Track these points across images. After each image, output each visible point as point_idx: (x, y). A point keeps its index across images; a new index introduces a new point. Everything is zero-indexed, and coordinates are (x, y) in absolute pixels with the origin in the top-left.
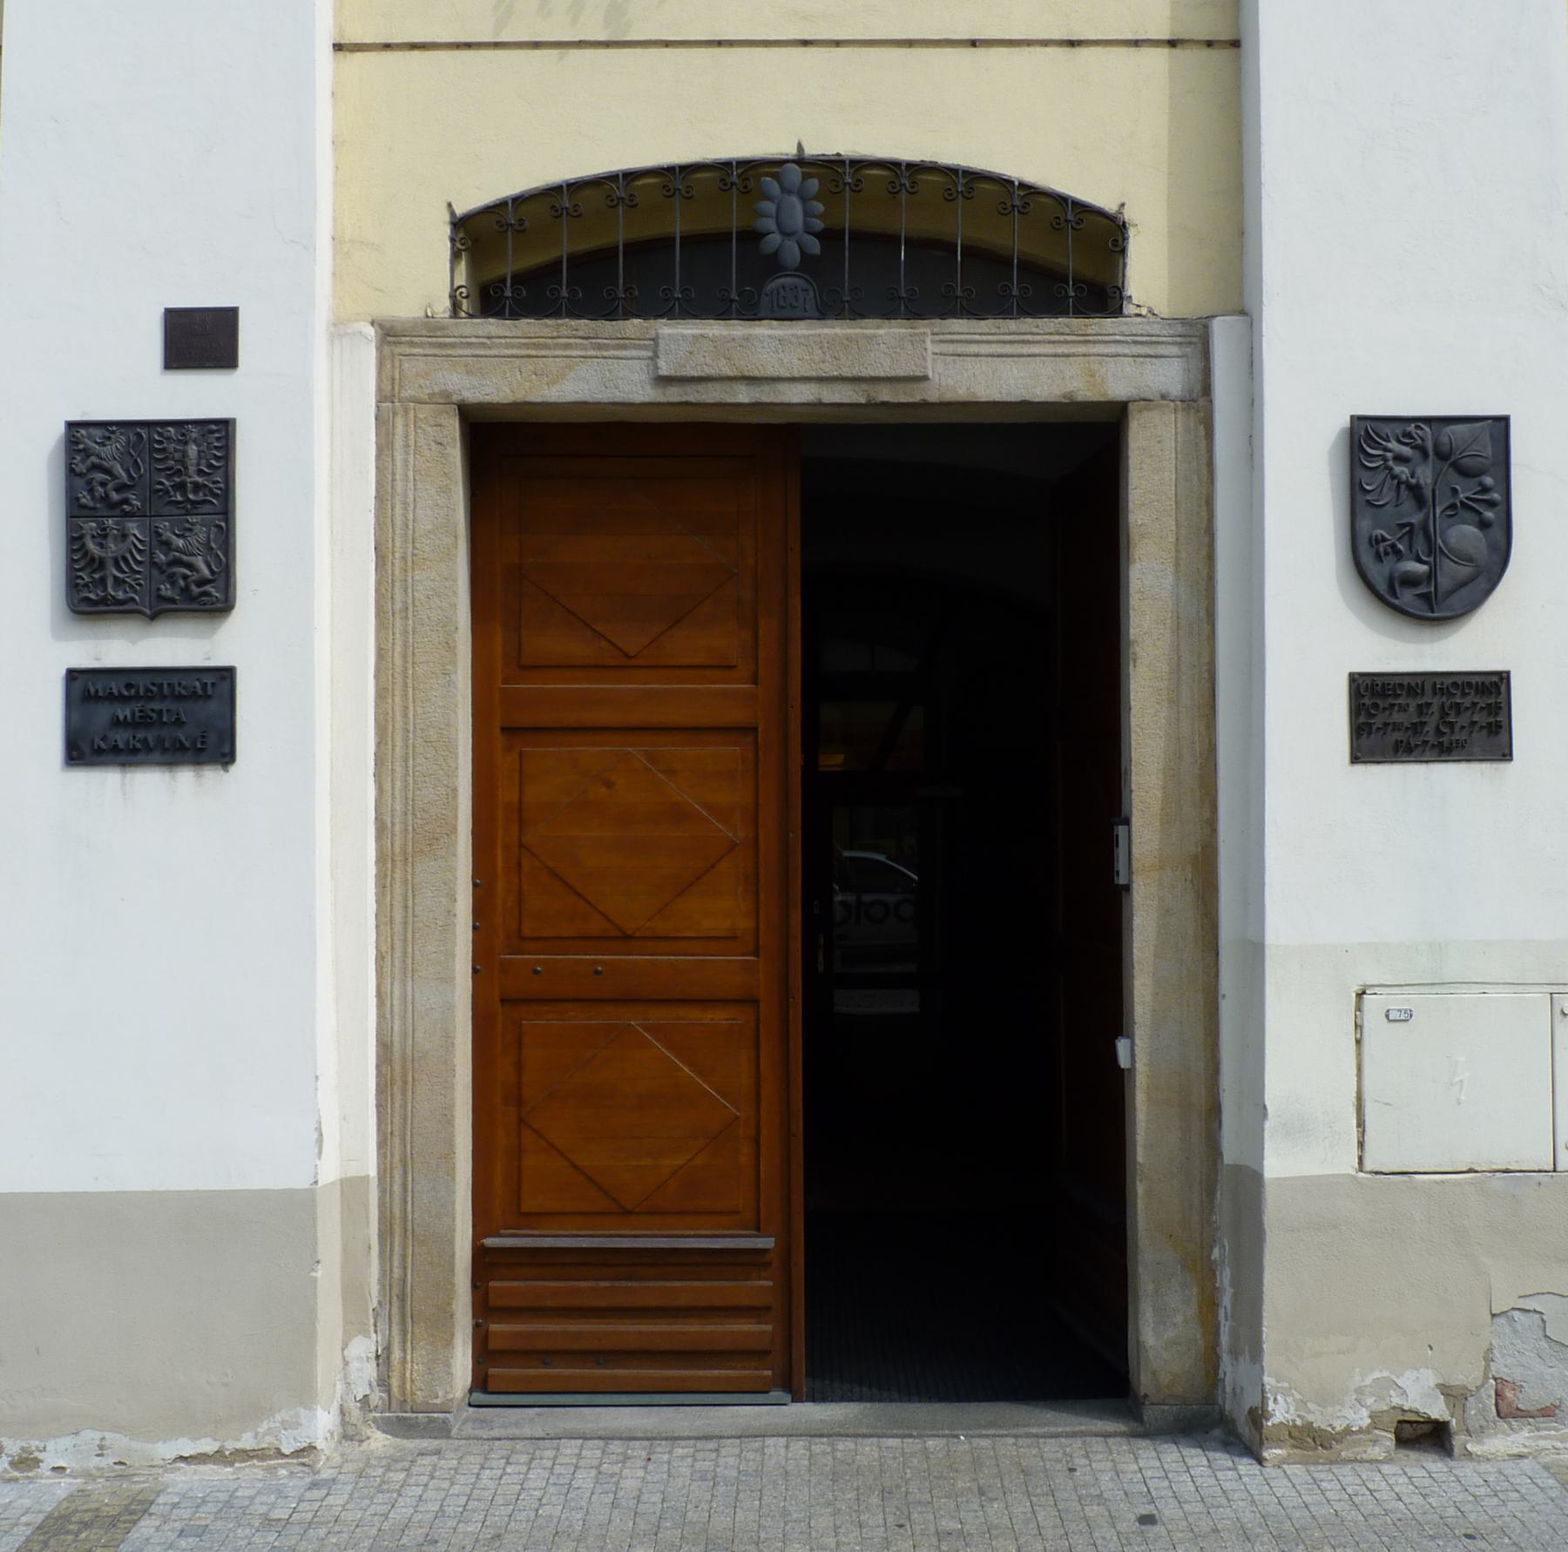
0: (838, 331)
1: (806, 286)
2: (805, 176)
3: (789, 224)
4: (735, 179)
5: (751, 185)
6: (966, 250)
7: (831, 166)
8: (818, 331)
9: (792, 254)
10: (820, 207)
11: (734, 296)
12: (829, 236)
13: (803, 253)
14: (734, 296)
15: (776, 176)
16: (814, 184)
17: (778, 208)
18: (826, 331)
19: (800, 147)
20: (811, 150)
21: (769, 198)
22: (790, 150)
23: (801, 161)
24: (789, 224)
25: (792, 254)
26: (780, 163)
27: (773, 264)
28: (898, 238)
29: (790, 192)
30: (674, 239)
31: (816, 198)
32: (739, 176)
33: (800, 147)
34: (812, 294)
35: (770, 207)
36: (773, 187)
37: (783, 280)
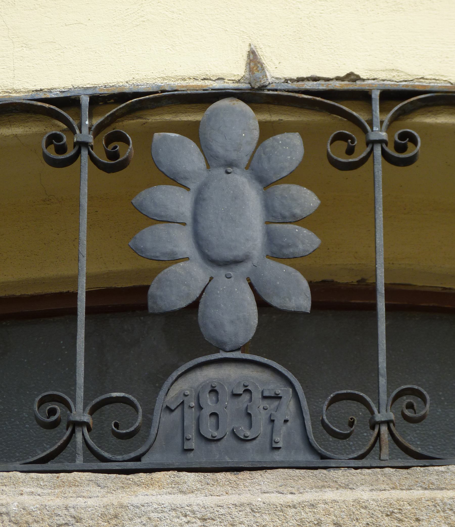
0: (364, 494)
1: (275, 386)
2: (267, 131)
3: (229, 240)
4: (85, 135)
5: (126, 151)
6: (390, 291)
7: (333, 106)
8: (310, 496)
9: (234, 315)
10: (307, 200)
11: (80, 413)
12: (340, 300)
13: (262, 305)
14: (80, 413)
15: (192, 131)
16: (290, 148)
17: (199, 201)
18: (330, 495)
19: (253, 60)
20: (285, 67)
21: (174, 180)
22: (229, 70)
23: (256, 96)
24: (229, 240)
25: (234, 315)
26: (204, 99)
27: (186, 332)
28: (368, 290)
29: (230, 165)
30: (372, 291)
31: (293, 178)
32: (97, 131)
33: (253, 60)
34: (288, 408)
35: (176, 201)
36: (184, 155)
37: (211, 374)
